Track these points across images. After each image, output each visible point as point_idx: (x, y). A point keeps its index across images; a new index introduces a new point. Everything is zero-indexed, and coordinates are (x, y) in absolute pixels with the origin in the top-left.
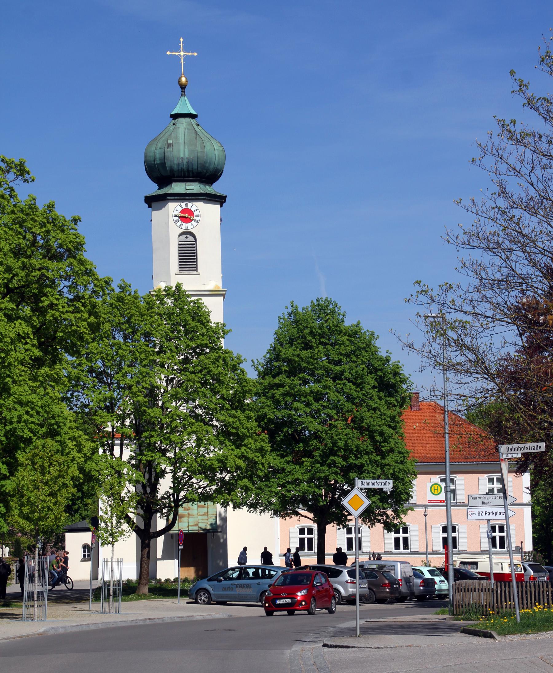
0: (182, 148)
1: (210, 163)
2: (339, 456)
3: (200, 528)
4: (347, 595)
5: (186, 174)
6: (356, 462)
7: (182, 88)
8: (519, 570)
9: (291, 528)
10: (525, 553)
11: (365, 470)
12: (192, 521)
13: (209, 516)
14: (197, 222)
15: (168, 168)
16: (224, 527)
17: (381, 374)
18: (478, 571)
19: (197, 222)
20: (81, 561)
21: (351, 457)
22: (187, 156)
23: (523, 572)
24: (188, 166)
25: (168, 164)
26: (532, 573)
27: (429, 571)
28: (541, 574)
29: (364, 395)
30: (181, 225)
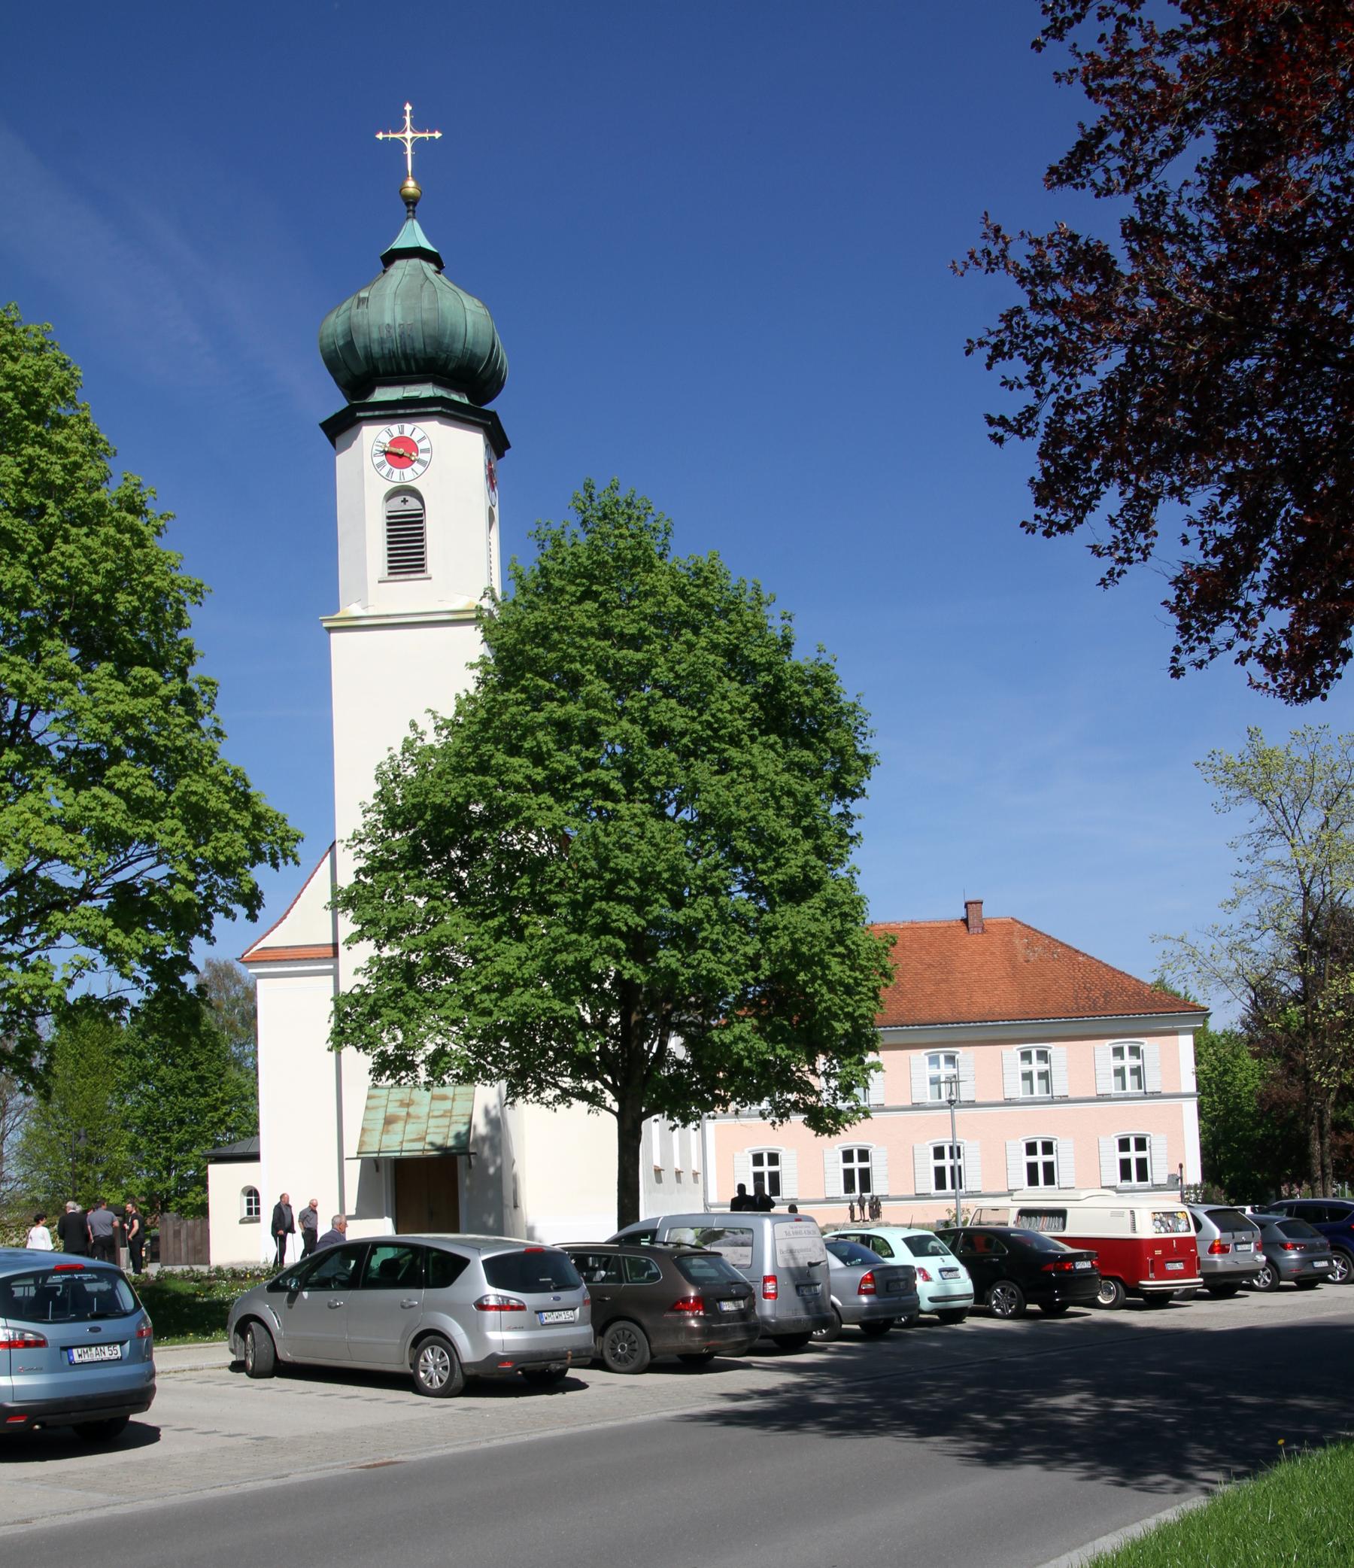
0: (388, 303)
1: (453, 336)
2: (622, 900)
3: (432, 1144)
4: (481, 1358)
5: (403, 366)
6: (672, 915)
7: (408, 204)
8: (1182, 1226)
9: (737, 1154)
10: (1189, 1187)
11: (705, 939)
12: (413, 1129)
13: (454, 1118)
14: (423, 463)
15: (361, 353)
16: (497, 1140)
17: (769, 678)
18: (1066, 1234)
19: (423, 463)
20: (242, 1222)
21: (657, 901)
22: (399, 321)
23: (1193, 1233)
24: (404, 345)
25: (359, 342)
26: (1217, 1233)
27: (908, 1241)
28: (1243, 1236)
29: (709, 725)
30: (390, 473)
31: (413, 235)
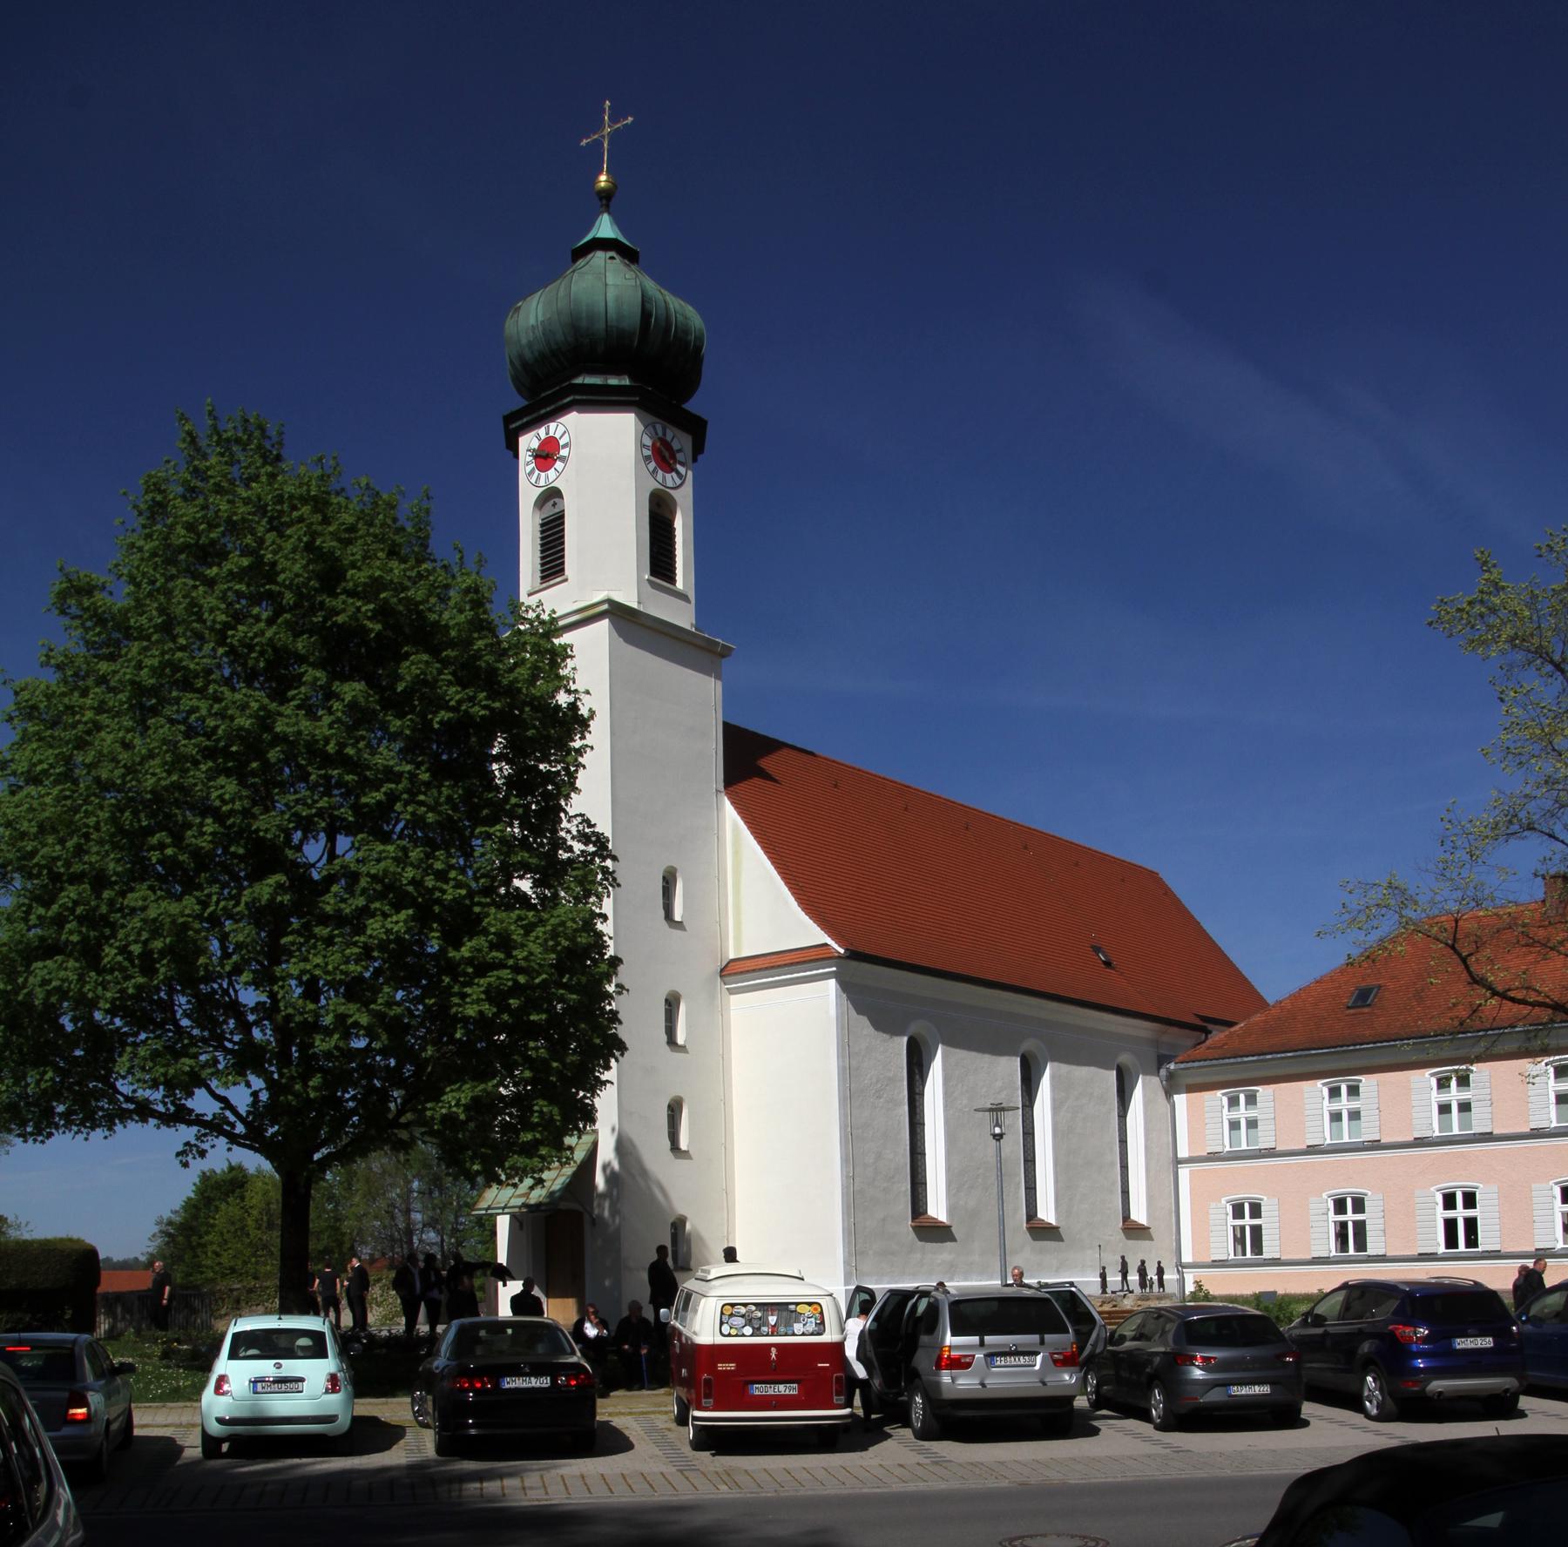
31: (605, 228)
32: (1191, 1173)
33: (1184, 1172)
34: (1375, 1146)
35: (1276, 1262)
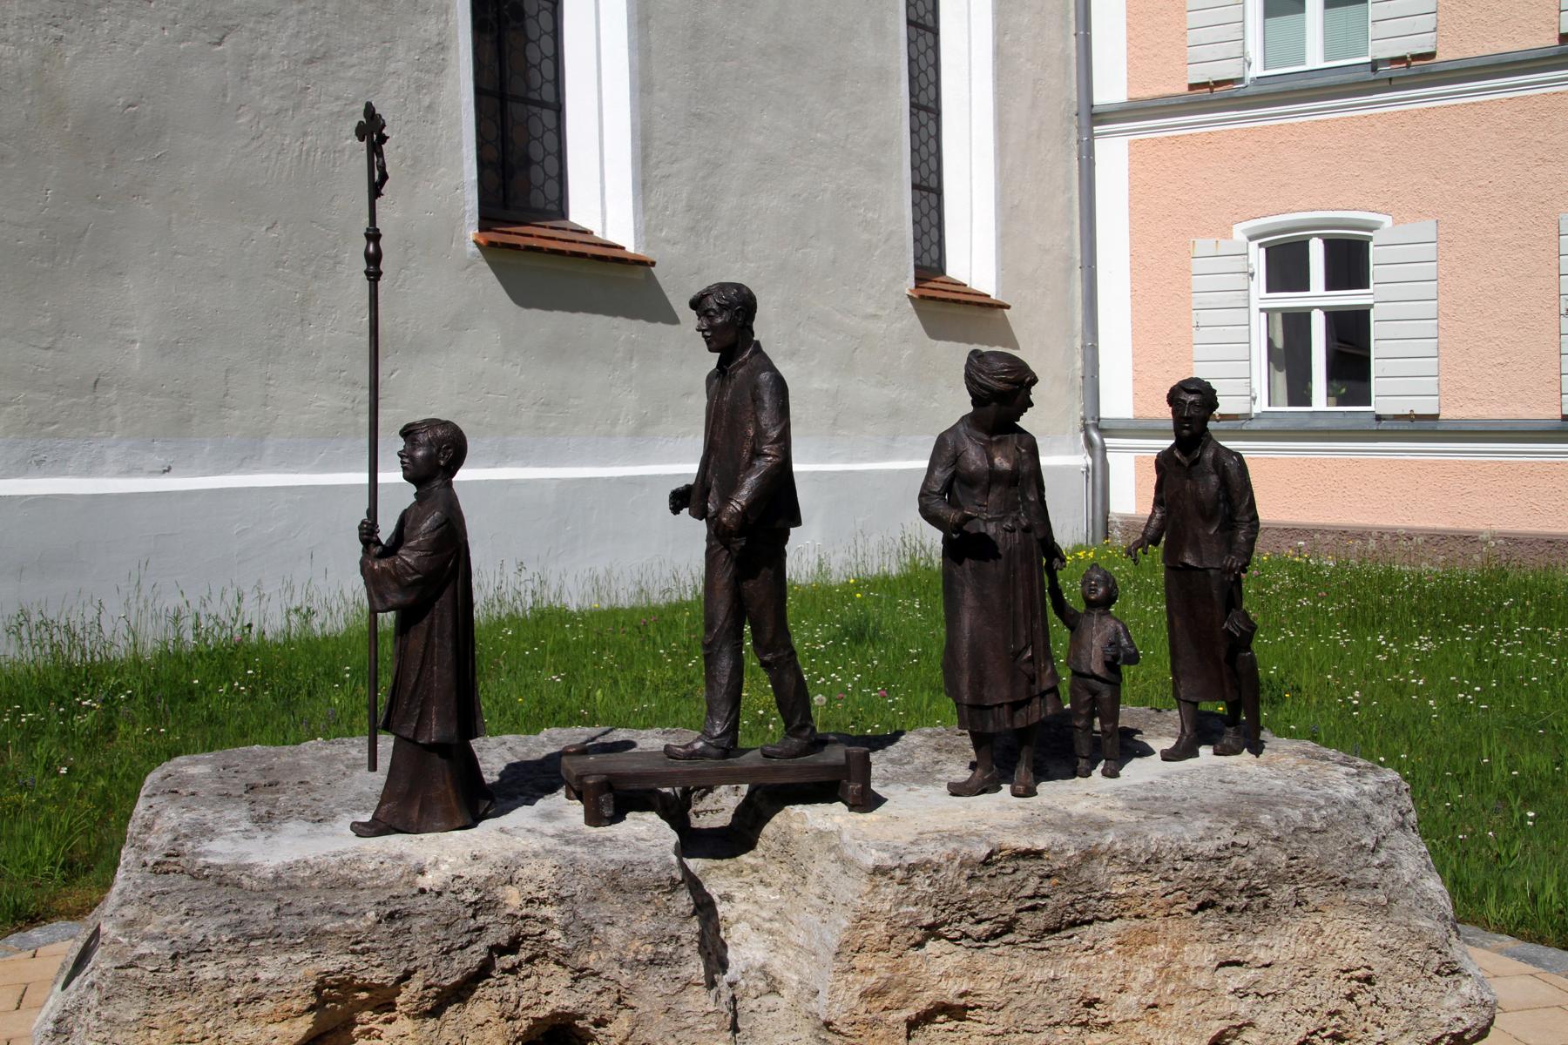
32: (1135, 150)
33: (1113, 153)
34: (1415, 71)
35: (1420, 427)
